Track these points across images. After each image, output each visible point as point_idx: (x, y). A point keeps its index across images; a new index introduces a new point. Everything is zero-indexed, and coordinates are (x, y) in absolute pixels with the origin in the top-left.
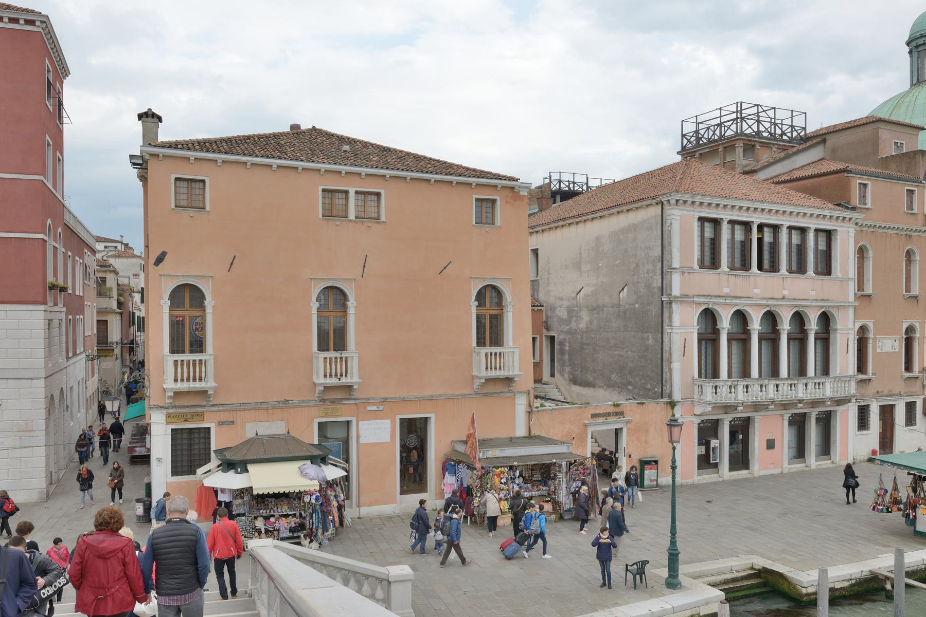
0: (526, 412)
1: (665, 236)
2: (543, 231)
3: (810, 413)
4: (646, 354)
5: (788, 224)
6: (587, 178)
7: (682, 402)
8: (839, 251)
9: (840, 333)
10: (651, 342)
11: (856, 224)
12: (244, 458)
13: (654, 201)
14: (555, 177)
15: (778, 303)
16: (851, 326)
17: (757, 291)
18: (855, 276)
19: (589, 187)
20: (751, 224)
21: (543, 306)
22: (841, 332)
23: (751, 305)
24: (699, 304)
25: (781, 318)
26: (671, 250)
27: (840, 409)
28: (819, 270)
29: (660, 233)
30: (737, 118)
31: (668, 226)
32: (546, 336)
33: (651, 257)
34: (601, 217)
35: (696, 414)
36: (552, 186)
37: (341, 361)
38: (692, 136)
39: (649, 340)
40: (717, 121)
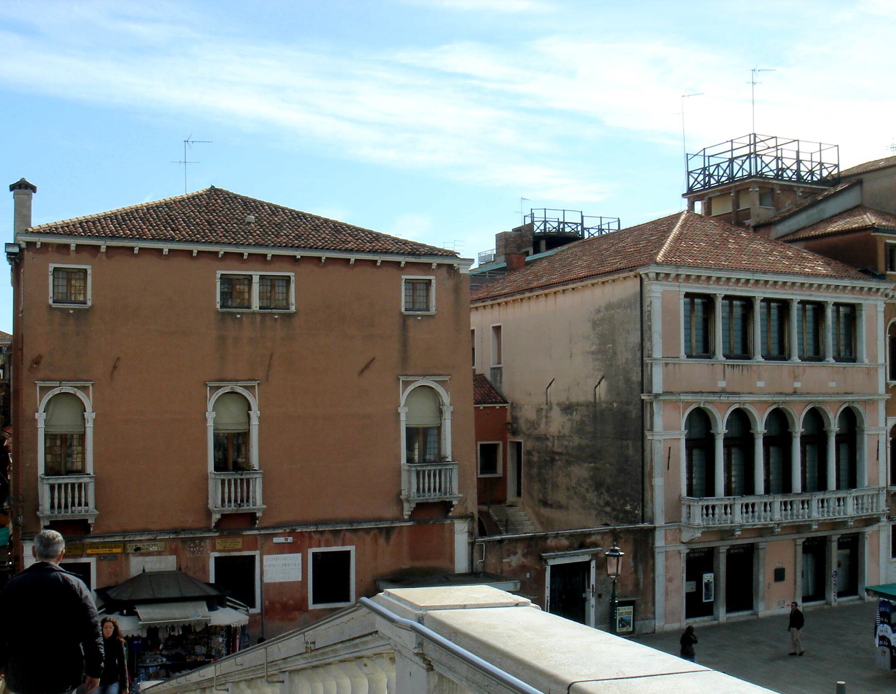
0: (468, 543)
1: (645, 318)
2: (506, 303)
3: (831, 536)
4: (625, 467)
5: (799, 298)
6: (582, 217)
7: (665, 527)
8: (864, 334)
9: (870, 435)
10: (631, 452)
11: (887, 296)
12: (131, 598)
13: (632, 274)
14: (539, 215)
15: (787, 399)
16: (882, 424)
17: (760, 384)
18: (886, 362)
19: (585, 229)
20: (753, 299)
21: (506, 402)
22: (868, 433)
23: (752, 403)
24: (690, 403)
25: (791, 414)
26: (651, 336)
27: (869, 530)
28: (842, 354)
29: (639, 313)
30: (750, 154)
31: (648, 306)
32: (510, 442)
33: (630, 343)
34: (573, 289)
35: (684, 541)
36: (535, 228)
37: (242, 484)
38: (700, 174)
39: (628, 449)
40: (729, 155)
